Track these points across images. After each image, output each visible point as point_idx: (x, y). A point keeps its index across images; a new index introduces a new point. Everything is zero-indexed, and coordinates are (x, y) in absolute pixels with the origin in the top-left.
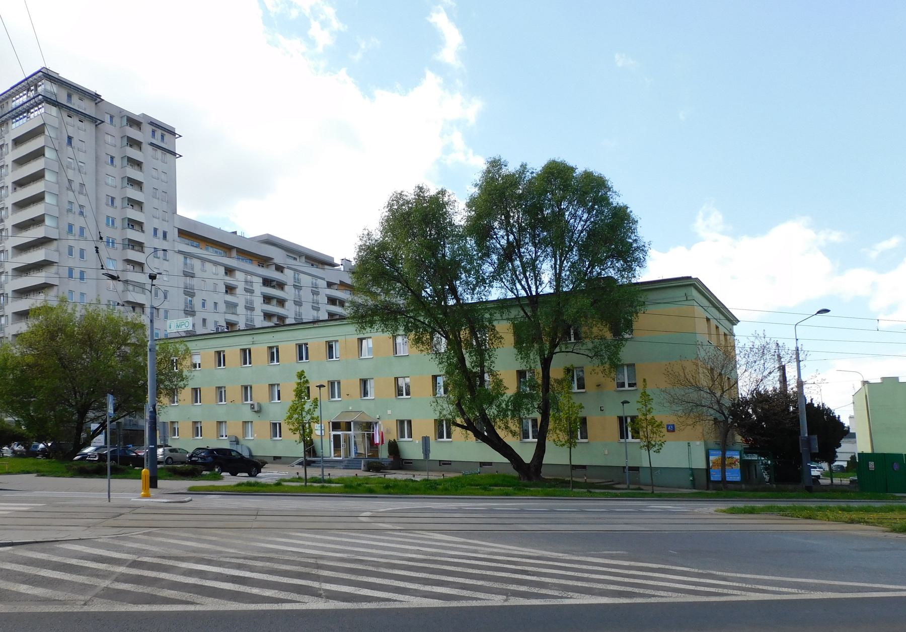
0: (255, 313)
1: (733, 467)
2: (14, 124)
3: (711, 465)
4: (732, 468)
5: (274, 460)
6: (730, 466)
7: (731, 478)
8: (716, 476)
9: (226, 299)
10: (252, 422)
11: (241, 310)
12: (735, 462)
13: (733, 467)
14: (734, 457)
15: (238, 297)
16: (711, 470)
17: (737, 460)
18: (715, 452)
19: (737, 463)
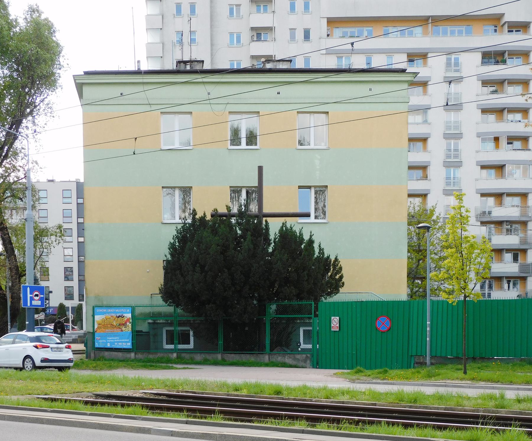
0: (462, 144)
1: (123, 329)
2: (5, 284)
3: (96, 327)
4: (122, 331)
5: (178, 32)
6: (120, 328)
7: (120, 344)
8: (100, 341)
9: (479, 187)
10: (239, 5)
11: (49, 250)
12: (126, 323)
13: (123, 329)
14: (125, 315)
15: (313, 235)
16: (96, 334)
17: (128, 320)
18: (101, 311)
19: (128, 324)
